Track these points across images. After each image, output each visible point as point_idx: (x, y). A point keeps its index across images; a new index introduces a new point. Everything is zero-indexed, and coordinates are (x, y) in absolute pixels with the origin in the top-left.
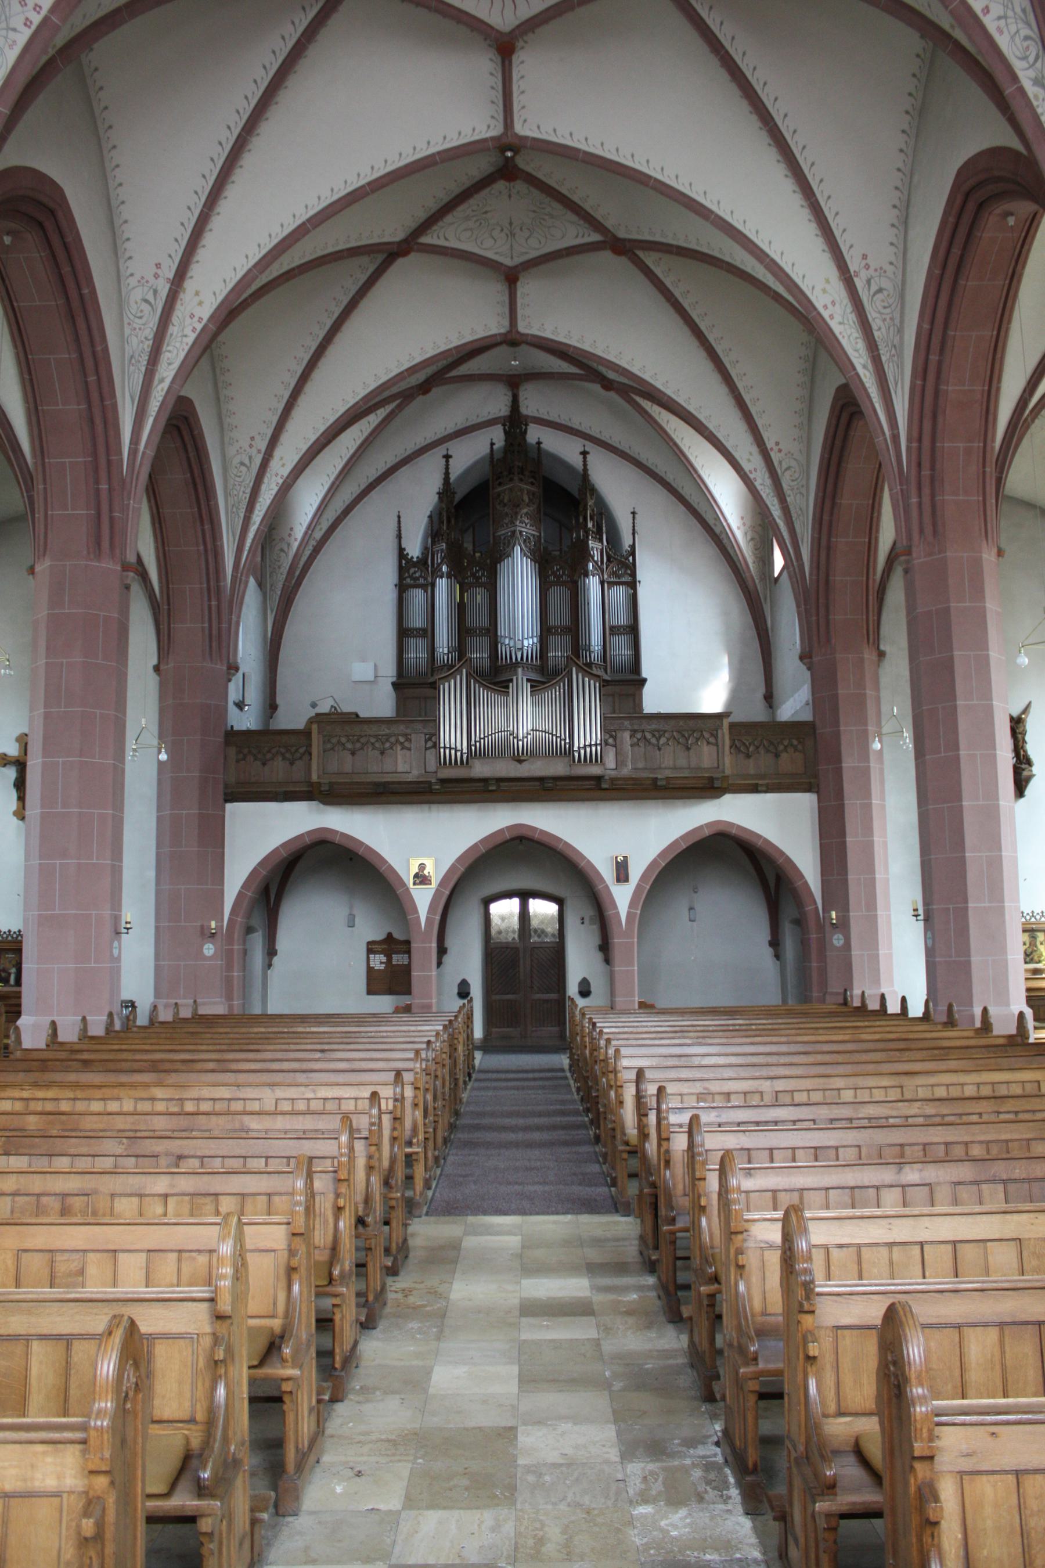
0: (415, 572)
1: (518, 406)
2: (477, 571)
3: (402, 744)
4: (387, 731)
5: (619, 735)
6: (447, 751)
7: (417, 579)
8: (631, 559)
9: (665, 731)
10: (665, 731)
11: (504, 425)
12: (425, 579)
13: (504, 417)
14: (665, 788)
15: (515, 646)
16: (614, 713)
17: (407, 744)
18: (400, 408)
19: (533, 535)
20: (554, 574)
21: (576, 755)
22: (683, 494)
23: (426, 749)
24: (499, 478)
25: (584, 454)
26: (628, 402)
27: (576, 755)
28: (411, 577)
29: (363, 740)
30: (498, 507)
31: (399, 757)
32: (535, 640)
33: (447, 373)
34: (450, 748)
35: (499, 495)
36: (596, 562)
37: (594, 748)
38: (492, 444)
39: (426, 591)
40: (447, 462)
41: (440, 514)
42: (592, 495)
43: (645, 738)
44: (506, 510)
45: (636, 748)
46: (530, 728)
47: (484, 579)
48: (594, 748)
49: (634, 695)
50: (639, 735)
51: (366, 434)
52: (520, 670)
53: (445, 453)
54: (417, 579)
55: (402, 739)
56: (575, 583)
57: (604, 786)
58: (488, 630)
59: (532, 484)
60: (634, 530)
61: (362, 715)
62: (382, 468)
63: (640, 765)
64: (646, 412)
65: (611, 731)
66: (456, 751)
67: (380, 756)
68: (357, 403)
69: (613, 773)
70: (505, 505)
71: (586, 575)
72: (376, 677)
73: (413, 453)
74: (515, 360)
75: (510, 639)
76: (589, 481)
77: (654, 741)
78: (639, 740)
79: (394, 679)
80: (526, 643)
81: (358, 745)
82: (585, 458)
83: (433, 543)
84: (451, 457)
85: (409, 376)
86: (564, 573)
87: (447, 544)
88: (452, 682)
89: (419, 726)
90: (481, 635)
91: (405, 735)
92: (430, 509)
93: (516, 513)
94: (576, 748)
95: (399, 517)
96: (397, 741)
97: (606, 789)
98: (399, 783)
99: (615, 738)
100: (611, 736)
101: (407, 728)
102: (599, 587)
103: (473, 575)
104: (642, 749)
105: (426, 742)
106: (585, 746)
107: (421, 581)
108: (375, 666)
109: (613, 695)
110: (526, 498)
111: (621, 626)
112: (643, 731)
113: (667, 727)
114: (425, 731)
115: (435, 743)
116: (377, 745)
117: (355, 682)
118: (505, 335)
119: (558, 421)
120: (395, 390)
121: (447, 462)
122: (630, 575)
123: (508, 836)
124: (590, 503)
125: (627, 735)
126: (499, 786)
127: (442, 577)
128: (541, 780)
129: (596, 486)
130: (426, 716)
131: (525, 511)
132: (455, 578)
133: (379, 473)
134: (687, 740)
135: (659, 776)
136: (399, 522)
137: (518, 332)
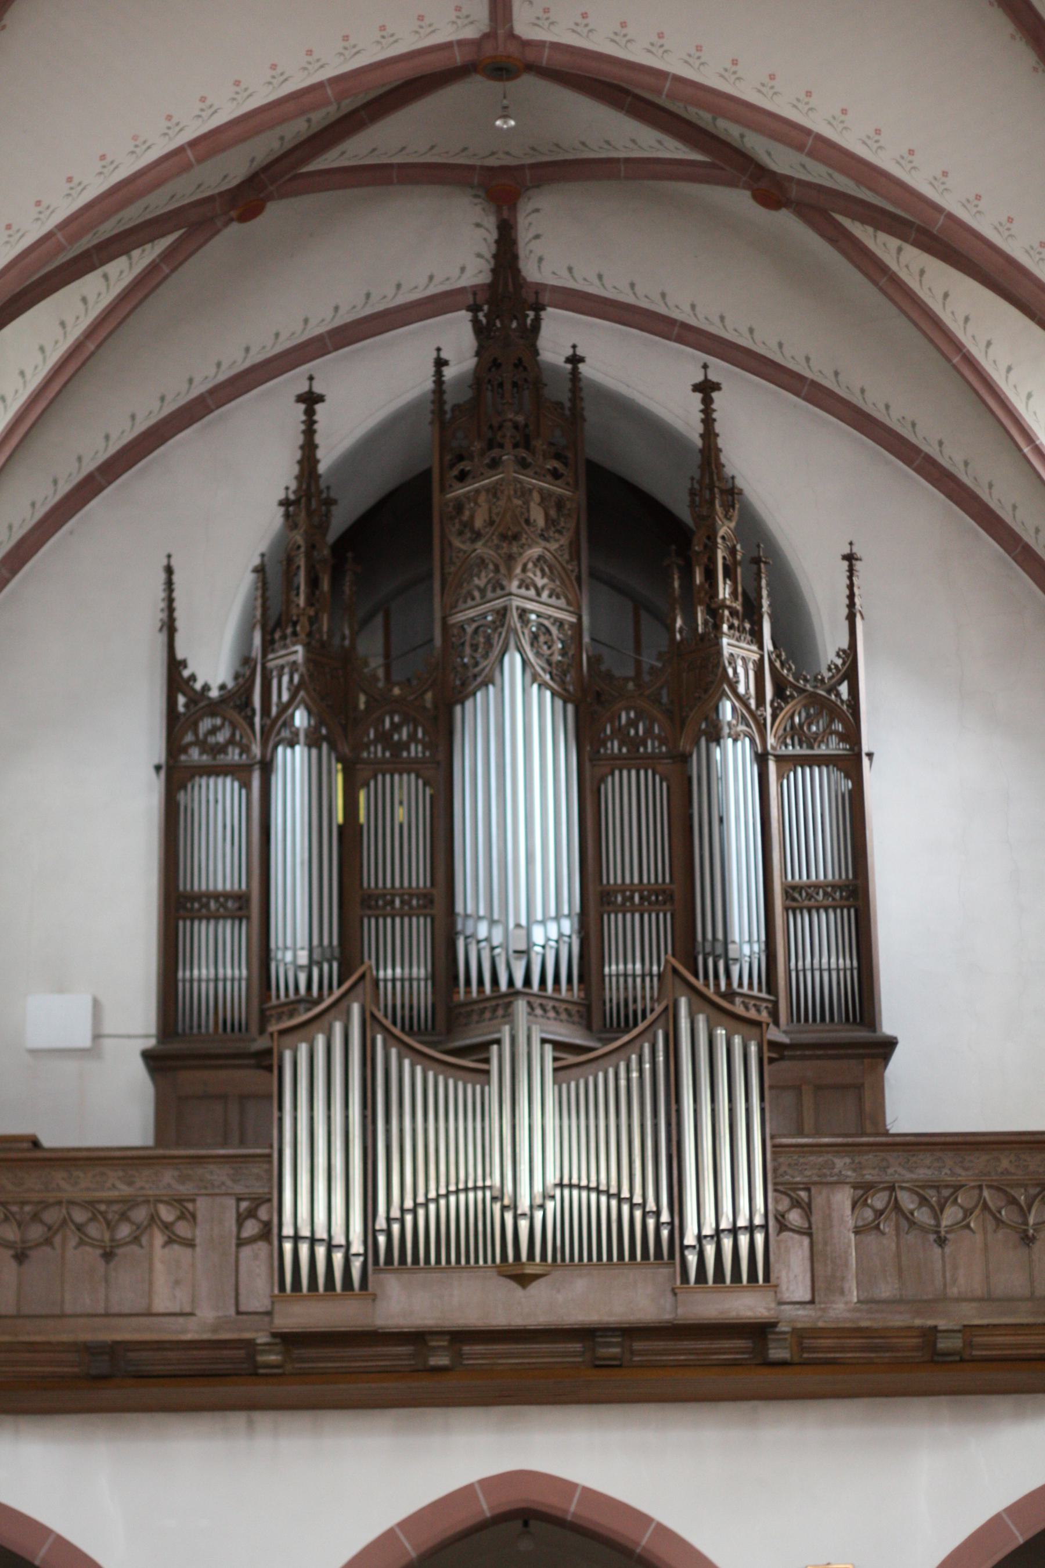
0: (214, 731)
1: (515, 257)
2: (396, 728)
3: (167, 1227)
4: (125, 1190)
5: (819, 1200)
6: (304, 1249)
7: (222, 749)
8: (844, 689)
9: (957, 1188)
10: (957, 1188)
11: (474, 309)
12: (245, 749)
13: (475, 290)
14: (961, 1359)
15: (505, 945)
16: (801, 1133)
17: (182, 1229)
18: (172, 258)
19: (560, 624)
20: (620, 733)
21: (692, 1258)
22: (993, 505)
23: (241, 1243)
24: (460, 458)
25: (706, 389)
26: (832, 241)
27: (692, 1258)
28: (202, 745)
29: (51, 1216)
30: (457, 543)
31: (159, 1266)
32: (567, 926)
33: (306, 160)
34: (313, 1241)
35: (459, 508)
36: (743, 701)
37: (744, 1240)
38: (440, 363)
39: (246, 785)
40: (310, 413)
41: (290, 560)
42: (729, 506)
43: (897, 1207)
44: (480, 548)
45: (871, 1239)
46: (552, 1179)
47: (415, 751)
48: (744, 1240)
49: (859, 1087)
50: (879, 1201)
51: (75, 333)
52: (521, 1006)
53: (304, 388)
54: (222, 749)
55: (166, 1214)
56: (685, 759)
57: (777, 1353)
58: (428, 899)
59: (556, 475)
60: (851, 605)
61: (47, 1142)
62: (123, 434)
63: (886, 1290)
64: (883, 269)
65: (795, 1187)
66: (330, 1248)
67: (101, 1263)
68: (49, 236)
69: (804, 1316)
70: (477, 536)
71: (715, 736)
72: (97, 1037)
73: (212, 392)
74: (505, 117)
75: (492, 922)
76: (720, 466)
77: (923, 1216)
78: (879, 1213)
79: (151, 1043)
80: (538, 935)
81: (36, 1232)
82: (707, 401)
83: (268, 645)
84: (320, 399)
85: (200, 160)
86: (649, 731)
87: (307, 646)
88: (320, 1040)
89: (220, 1174)
90: (405, 914)
91: (178, 1202)
92: (263, 547)
93: (510, 559)
94: (690, 1239)
95: (169, 570)
96: (154, 1218)
97: (783, 1364)
98: (159, 1346)
99: (807, 1209)
100: (796, 1203)
101: (183, 1179)
102: (752, 771)
103: (384, 738)
104: (889, 1243)
105: (240, 1221)
106: (718, 1232)
107: (234, 755)
108: (96, 1004)
109: (797, 1089)
110: (538, 517)
111: (817, 886)
112: (892, 1188)
113: (962, 1176)
114: (239, 1189)
115: (267, 1225)
116: (93, 1230)
117: (34, 1052)
118: (476, 44)
119: (629, 299)
120: (158, 203)
121: (310, 413)
122: (842, 737)
123: (486, 1508)
124: (725, 529)
125: (843, 1198)
126: (459, 1356)
127: (292, 745)
128: (587, 1334)
129: (740, 483)
130: (242, 1143)
131: (535, 551)
132: (333, 747)
133: (113, 449)
134: (1024, 1213)
135: (942, 1324)
136: (169, 585)
137: (512, 36)
